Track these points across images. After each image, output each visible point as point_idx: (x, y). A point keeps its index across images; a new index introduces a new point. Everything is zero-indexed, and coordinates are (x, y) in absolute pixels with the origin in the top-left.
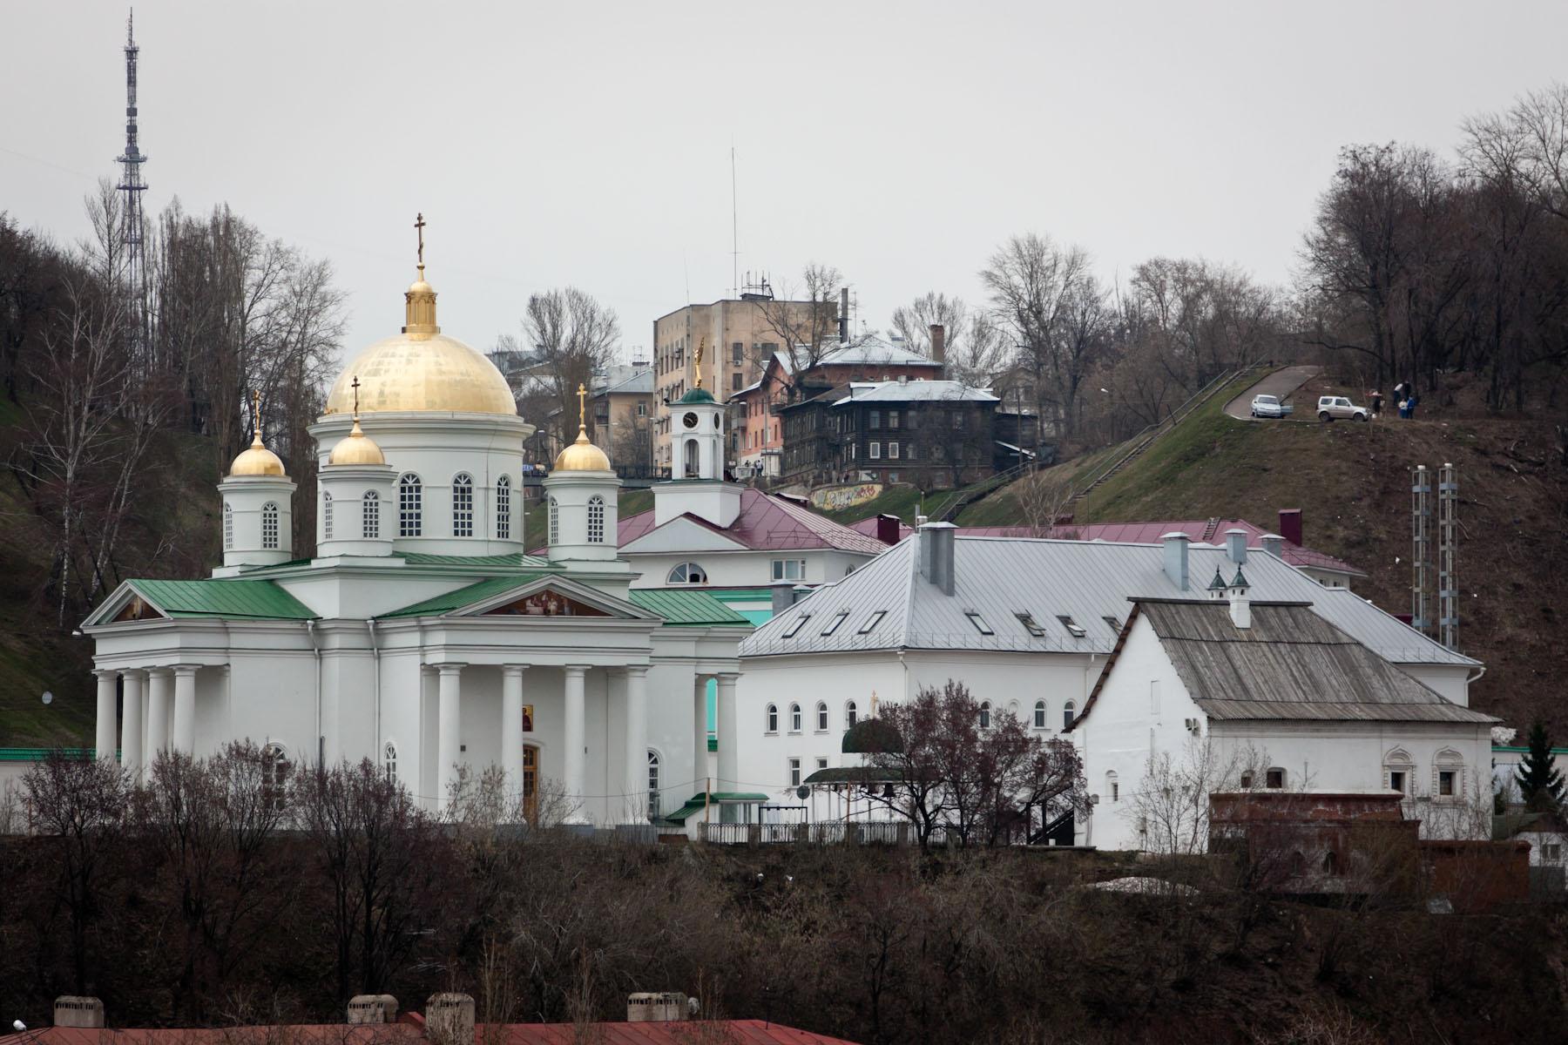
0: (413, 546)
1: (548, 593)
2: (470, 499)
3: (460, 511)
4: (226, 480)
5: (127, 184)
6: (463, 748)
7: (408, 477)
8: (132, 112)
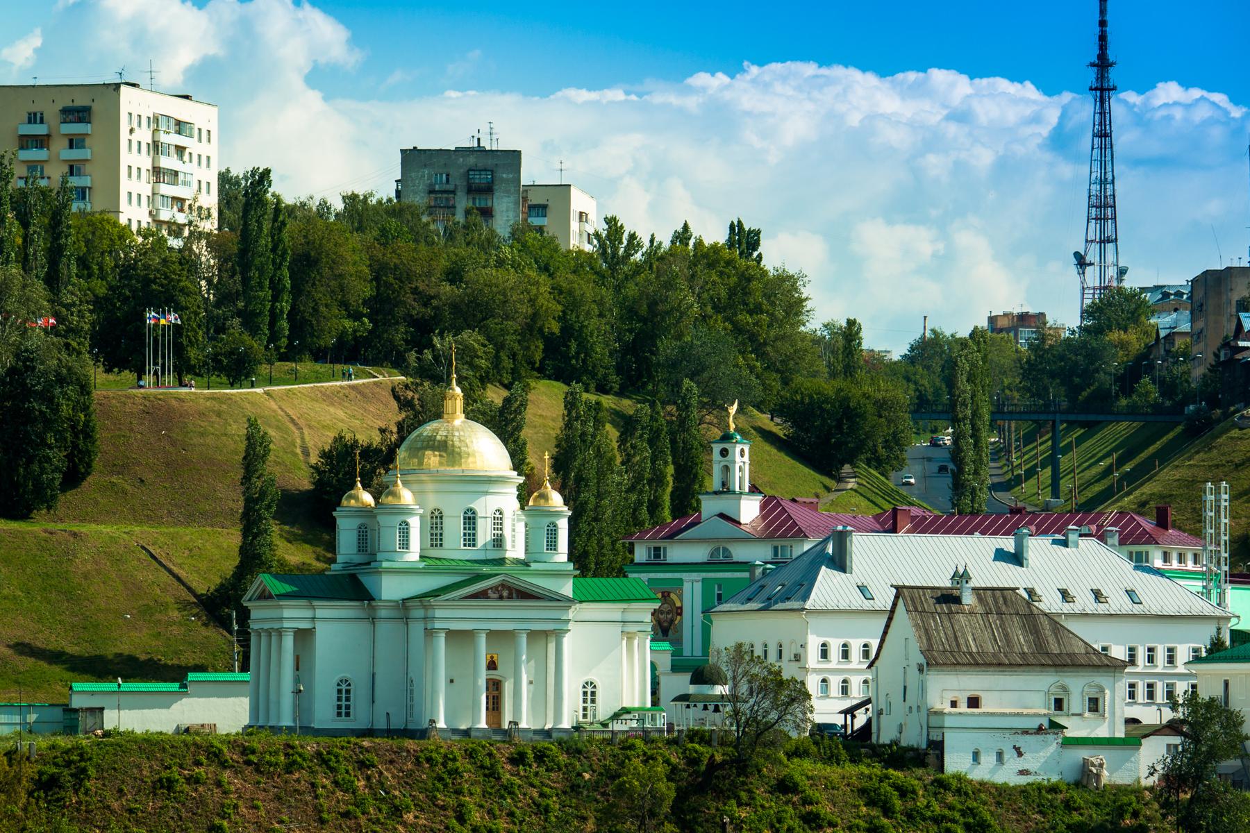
1: (503, 585)
2: (474, 524)
3: (467, 531)
4: (338, 509)
5: (1099, 85)
6: (452, 681)
8: (1103, 23)
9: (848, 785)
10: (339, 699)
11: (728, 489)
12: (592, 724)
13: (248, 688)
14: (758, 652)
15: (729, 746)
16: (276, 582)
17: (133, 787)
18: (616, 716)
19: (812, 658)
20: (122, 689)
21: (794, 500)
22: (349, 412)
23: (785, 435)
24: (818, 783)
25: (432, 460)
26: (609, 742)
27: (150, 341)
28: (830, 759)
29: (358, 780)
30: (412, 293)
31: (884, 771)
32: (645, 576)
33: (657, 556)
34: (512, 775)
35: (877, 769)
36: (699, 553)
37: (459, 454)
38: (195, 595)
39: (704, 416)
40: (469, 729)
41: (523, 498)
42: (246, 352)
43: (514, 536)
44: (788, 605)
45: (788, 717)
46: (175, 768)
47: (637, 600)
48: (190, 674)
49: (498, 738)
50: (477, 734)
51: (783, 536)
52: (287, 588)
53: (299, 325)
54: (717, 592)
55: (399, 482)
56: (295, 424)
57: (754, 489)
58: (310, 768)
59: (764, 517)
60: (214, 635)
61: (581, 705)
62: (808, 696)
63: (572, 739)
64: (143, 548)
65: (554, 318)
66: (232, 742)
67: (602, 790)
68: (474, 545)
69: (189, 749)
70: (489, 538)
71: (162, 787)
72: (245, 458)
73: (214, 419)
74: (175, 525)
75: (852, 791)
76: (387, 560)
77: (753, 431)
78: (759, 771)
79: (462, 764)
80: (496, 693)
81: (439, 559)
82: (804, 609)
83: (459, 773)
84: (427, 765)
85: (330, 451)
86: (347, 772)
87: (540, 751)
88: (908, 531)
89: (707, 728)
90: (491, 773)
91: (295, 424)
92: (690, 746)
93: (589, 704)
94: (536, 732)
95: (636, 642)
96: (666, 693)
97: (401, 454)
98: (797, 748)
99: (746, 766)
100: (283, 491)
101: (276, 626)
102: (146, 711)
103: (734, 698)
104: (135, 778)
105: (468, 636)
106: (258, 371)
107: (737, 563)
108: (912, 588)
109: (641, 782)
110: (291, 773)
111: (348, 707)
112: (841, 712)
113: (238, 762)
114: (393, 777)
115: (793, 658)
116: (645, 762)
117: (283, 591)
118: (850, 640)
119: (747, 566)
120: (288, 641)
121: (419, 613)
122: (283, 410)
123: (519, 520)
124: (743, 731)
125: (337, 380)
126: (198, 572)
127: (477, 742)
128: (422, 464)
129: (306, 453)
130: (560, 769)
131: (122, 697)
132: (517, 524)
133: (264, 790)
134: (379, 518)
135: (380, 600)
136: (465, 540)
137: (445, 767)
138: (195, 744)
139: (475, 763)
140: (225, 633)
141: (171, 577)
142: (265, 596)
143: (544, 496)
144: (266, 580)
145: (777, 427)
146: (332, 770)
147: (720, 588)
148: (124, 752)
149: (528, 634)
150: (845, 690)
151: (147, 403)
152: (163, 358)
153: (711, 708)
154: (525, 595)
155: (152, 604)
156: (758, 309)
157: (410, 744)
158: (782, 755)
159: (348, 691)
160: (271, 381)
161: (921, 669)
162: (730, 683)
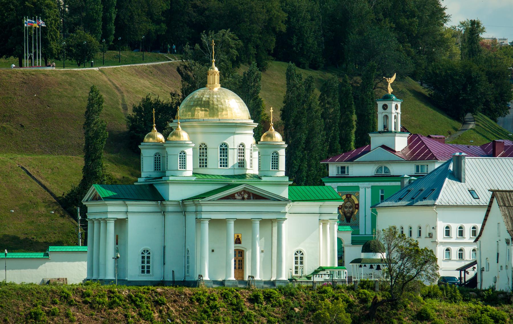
1: (245, 191)
2: (226, 153)
3: (222, 158)
4: (142, 144)
6: (213, 251)
7: (225, 144)
9: (462, 315)
10: (143, 262)
11: (387, 130)
12: (301, 277)
13: (86, 256)
14: (406, 233)
15: (386, 290)
16: (103, 190)
17: (13, 318)
18: (316, 272)
19: (440, 235)
20: (7, 257)
21: (429, 137)
22: (152, 82)
23: (429, 94)
24: (442, 314)
25: (200, 114)
26: (311, 288)
27: (26, 38)
28: (450, 299)
29: (154, 313)
30: (192, 7)
31: (485, 307)
32: (335, 185)
33: (343, 172)
34: (250, 309)
35: (480, 306)
36: (370, 170)
37: (217, 109)
38: (56, 198)
39: (377, 83)
40: (224, 281)
41: (257, 135)
42: (87, 45)
43: (251, 160)
44: (425, 202)
45: (423, 272)
46: (39, 306)
47: (329, 200)
48: (50, 247)
49: (242, 286)
50: (229, 284)
51: (422, 159)
52: (111, 193)
53: (120, 27)
54: (380, 194)
55: (179, 127)
56: (119, 90)
57: (404, 130)
58: (124, 305)
59: (410, 147)
60: (66, 222)
61: (294, 265)
62: (435, 259)
63: (288, 286)
64: (22, 168)
65: (282, 22)
66: (76, 290)
67: (306, 319)
68: (226, 166)
69: (48, 294)
70: (236, 161)
71: (31, 318)
72: (86, 112)
73: (67, 86)
74: (43, 153)
75: (464, 319)
76: (172, 176)
77: (408, 91)
78: (405, 306)
79: (219, 302)
80: (240, 258)
81: (205, 175)
82: (434, 205)
83: (217, 308)
84: (197, 303)
85: (140, 107)
86: (147, 308)
87: (268, 294)
88: (503, 156)
89: (373, 279)
90: (237, 308)
91: (119, 90)
92: (362, 291)
93: (299, 265)
94: (265, 282)
95: (328, 226)
96: (348, 258)
97: (181, 109)
98: (429, 292)
99: (397, 303)
100: (110, 132)
101: (103, 217)
102: (22, 270)
103: (389, 261)
104: (14, 312)
105: (222, 223)
106: (95, 57)
107: (393, 176)
108: (502, 191)
109: (330, 313)
110: (112, 308)
111: (148, 267)
112: (457, 270)
113: (79, 302)
114: (176, 311)
115: (428, 236)
116: (332, 301)
117: (107, 195)
118: (463, 224)
119: (399, 178)
120: (111, 226)
121: (192, 208)
122: (110, 81)
123: (255, 150)
124: (395, 281)
125: (146, 62)
126: (57, 183)
127: (228, 288)
128: (194, 115)
129: (125, 108)
130: (280, 306)
131: (8, 262)
132: (253, 153)
133: (96, 319)
134: (167, 149)
135: (168, 200)
136: (221, 163)
137: (208, 304)
138: (52, 291)
139: (227, 302)
140: (74, 221)
141: (40, 186)
142: (96, 198)
143: (270, 136)
144: (96, 188)
145: (424, 90)
146: (138, 306)
147: (382, 192)
148: (7, 296)
149: (260, 222)
150: (461, 256)
151: (25, 77)
152: (35, 48)
153: (375, 267)
154: (258, 197)
155: (28, 203)
156: (413, 15)
157: (187, 290)
158: (419, 296)
159: (148, 258)
160: (104, 63)
161: (508, 243)
162: (387, 251)
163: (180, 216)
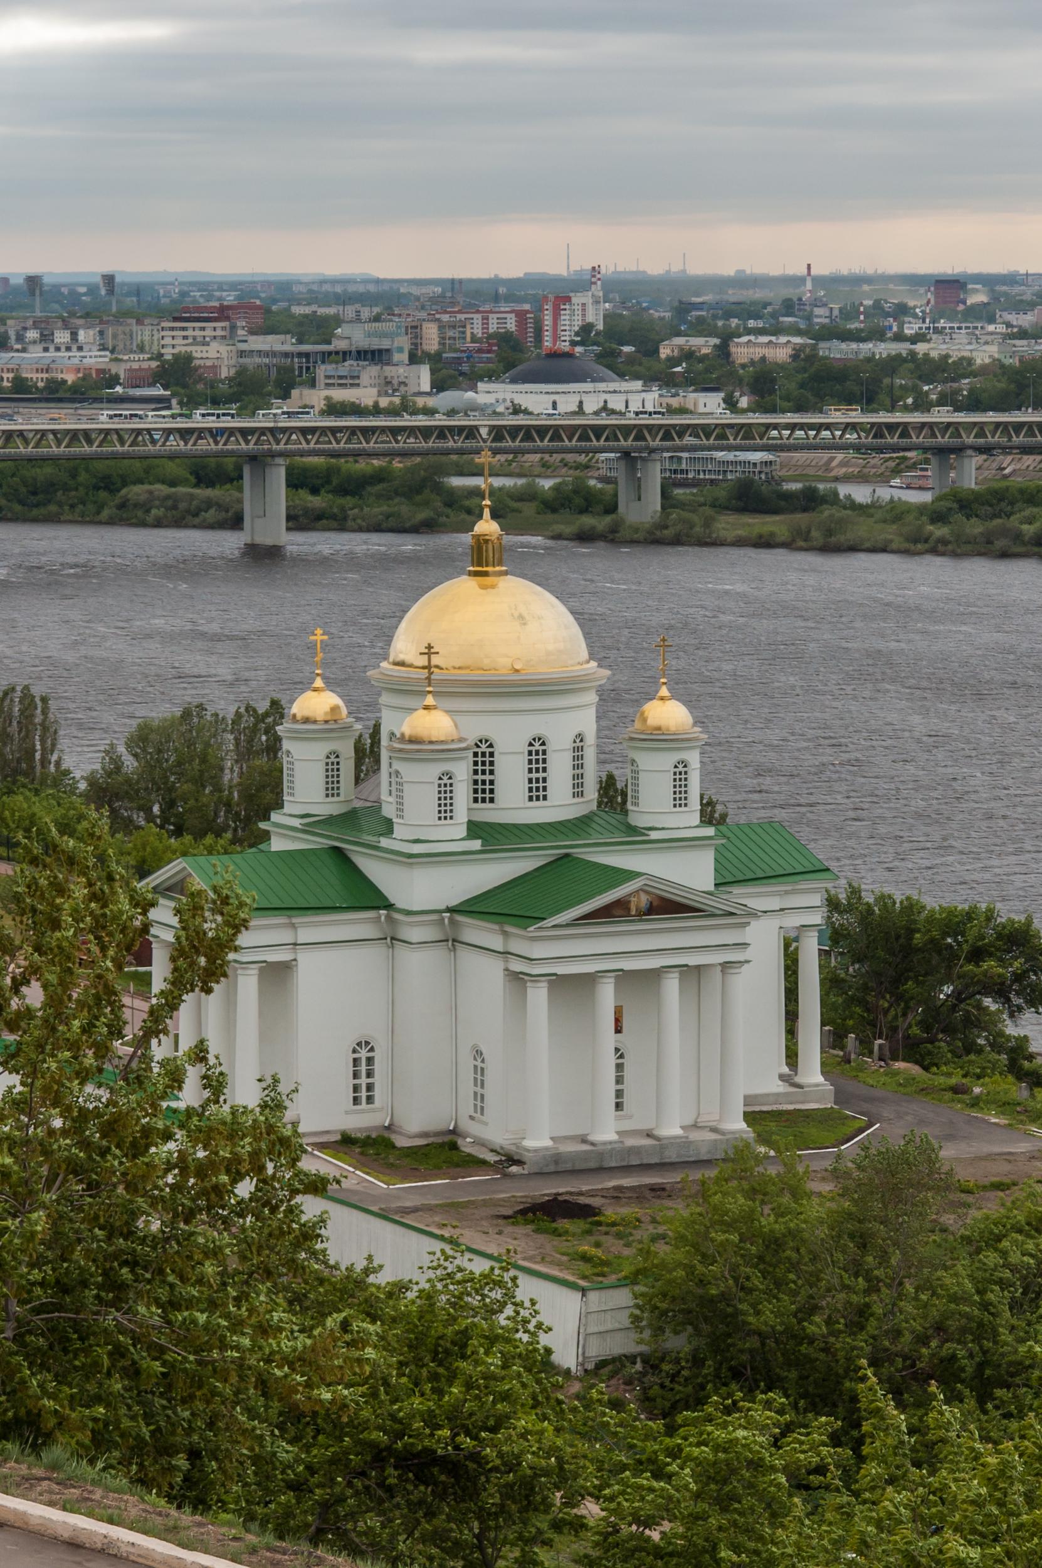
0: (488, 814)
3: (487, 777)
10: (356, 1075)
159: (370, 1061)
163: (438, 954)
